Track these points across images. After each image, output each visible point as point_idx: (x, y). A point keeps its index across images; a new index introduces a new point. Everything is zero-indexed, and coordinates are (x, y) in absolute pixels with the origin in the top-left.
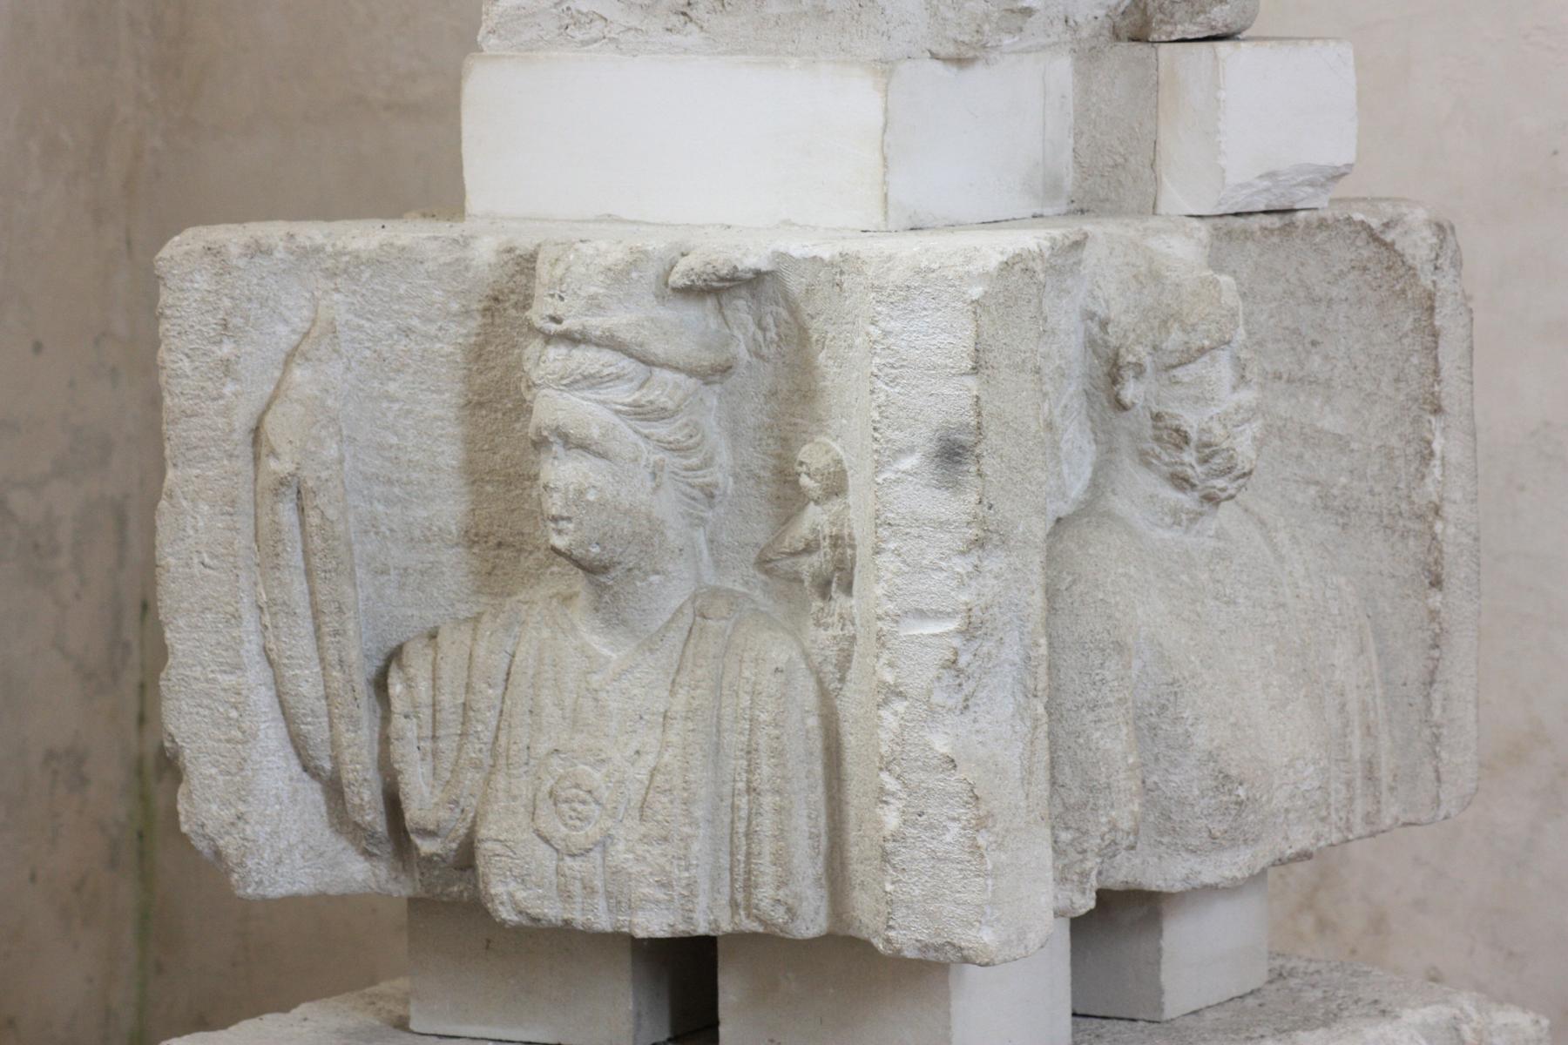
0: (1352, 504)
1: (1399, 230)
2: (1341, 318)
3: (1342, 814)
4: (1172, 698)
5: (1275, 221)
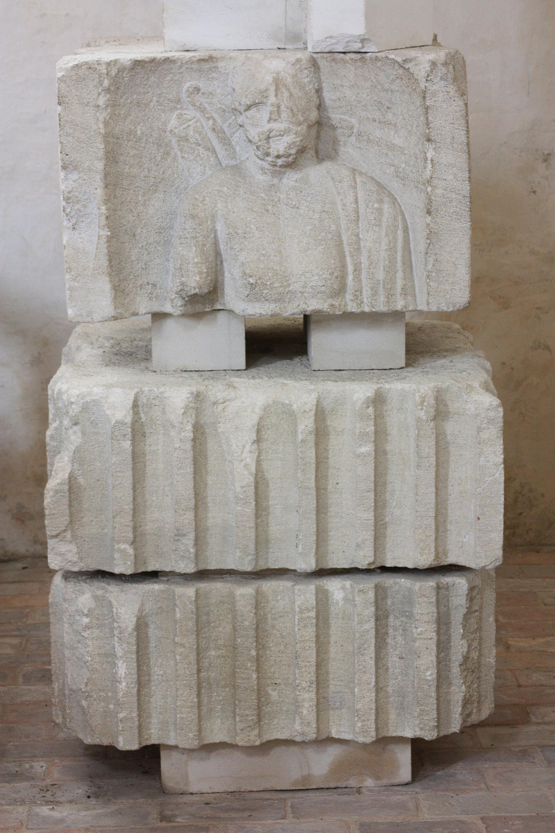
0: (406, 176)
1: (413, 63)
2: (397, 98)
3: (369, 300)
4: (229, 240)
5: (359, 56)
